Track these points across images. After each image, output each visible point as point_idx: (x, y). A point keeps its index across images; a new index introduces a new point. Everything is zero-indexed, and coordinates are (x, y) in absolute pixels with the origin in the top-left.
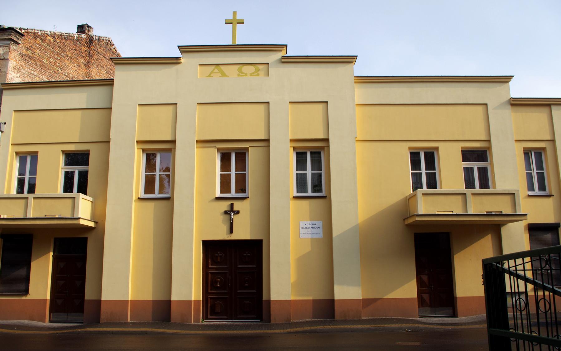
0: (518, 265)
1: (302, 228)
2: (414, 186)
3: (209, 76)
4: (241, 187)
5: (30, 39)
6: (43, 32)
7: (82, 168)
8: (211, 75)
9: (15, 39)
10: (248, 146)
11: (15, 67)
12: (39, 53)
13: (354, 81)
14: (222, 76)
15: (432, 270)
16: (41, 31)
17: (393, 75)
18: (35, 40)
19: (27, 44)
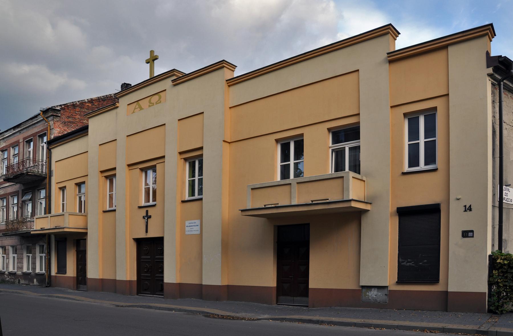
1: (187, 226)
3: (134, 112)
4: (431, 158)
5: (70, 110)
6: (81, 102)
7: (353, 144)
8: (134, 112)
10: (156, 164)
12: (79, 117)
13: (227, 85)
14: (140, 110)
15: (293, 261)
16: (78, 102)
18: (74, 109)
19: (68, 114)
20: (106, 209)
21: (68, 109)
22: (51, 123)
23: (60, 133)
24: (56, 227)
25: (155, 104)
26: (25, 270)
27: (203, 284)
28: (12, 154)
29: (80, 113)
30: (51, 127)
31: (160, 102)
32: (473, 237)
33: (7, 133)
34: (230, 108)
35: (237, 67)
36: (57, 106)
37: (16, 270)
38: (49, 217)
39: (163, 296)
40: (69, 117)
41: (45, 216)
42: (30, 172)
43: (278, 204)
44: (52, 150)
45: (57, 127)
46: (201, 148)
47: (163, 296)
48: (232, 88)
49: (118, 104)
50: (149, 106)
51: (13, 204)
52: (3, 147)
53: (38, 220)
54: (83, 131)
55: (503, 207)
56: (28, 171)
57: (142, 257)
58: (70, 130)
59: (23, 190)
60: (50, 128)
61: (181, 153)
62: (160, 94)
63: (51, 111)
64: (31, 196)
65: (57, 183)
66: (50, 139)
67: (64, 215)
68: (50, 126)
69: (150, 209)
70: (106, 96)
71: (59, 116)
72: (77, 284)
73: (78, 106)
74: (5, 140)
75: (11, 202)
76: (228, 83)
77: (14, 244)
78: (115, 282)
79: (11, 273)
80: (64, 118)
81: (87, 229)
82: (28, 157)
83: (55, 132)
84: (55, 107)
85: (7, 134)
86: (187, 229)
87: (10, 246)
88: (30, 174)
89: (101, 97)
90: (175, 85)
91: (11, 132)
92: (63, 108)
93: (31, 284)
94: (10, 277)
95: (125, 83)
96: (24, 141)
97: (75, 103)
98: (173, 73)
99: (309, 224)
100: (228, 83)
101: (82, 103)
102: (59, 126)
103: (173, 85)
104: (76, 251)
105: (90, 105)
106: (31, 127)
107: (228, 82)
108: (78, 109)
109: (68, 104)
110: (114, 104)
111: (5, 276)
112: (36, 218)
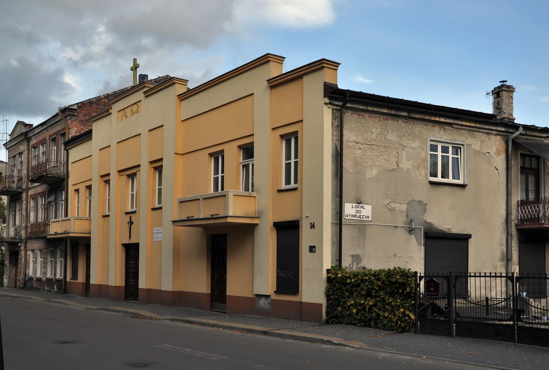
0: (491, 301)
2: (436, 165)
3: (122, 120)
9: (72, 113)
11: (77, 131)
13: (178, 100)
17: (253, 60)
19: (84, 112)
20: (106, 214)
21: (85, 107)
22: (69, 122)
23: (77, 133)
24: (65, 231)
25: (135, 113)
26: (49, 276)
27: (303, 301)
28: (41, 152)
29: (96, 110)
30: (69, 126)
31: (138, 112)
32: (315, 252)
33: (36, 130)
34: (182, 121)
35: (188, 81)
36: (74, 105)
37: (41, 276)
38: (61, 221)
39: (138, 302)
40: (86, 115)
41: (55, 221)
42: (49, 174)
43: (193, 217)
44: (69, 151)
45: (74, 127)
46: (161, 160)
47: (138, 302)
48: (184, 103)
49: (111, 111)
50: (132, 115)
51: (41, 205)
52: (34, 144)
53: (53, 223)
54: (87, 136)
55: (343, 223)
56: (48, 173)
57: (129, 263)
58: (87, 129)
59: (49, 191)
60: (68, 127)
61: (151, 162)
62: (138, 103)
63: (68, 111)
64: (54, 198)
65: (73, 185)
66: (68, 138)
67: (70, 219)
68: (68, 125)
69: (132, 215)
70: (122, 89)
71: (76, 115)
72: (212, 302)
73: (94, 103)
74: (36, 136)
75: (40, 202)
76: (179, 98)
77: (41, 248)
78: (160, 292)
79: (58, 280)
80: (81, 117)
81: (90, 233)
82: (47, 159)
83: (73, 131)
84: (72, 106)
85: (36, 131)
86: (155, 235)
87: (38, 249)
88: (49, 176)
89: (117, 91)
90: (147, 97)
91: (39, 129)
92: (80, 106)
93: (52, 291)
94: (37, 283)
95: (141, 75)
96: (49, 139)
97: (92, 100)
98: (144, 85)
99: (226, 234)
100: (179, 98)
101: (98, 99)
102: (76, 125)
103: (145, 96)
104: (86, 255)
105: (106, 101)
106: (55, 125)
107: (179, 97)
108: (94, 106)
109: (85, 102)
110: (108, 111)
111: (34, 282)
112: (52, 222)
